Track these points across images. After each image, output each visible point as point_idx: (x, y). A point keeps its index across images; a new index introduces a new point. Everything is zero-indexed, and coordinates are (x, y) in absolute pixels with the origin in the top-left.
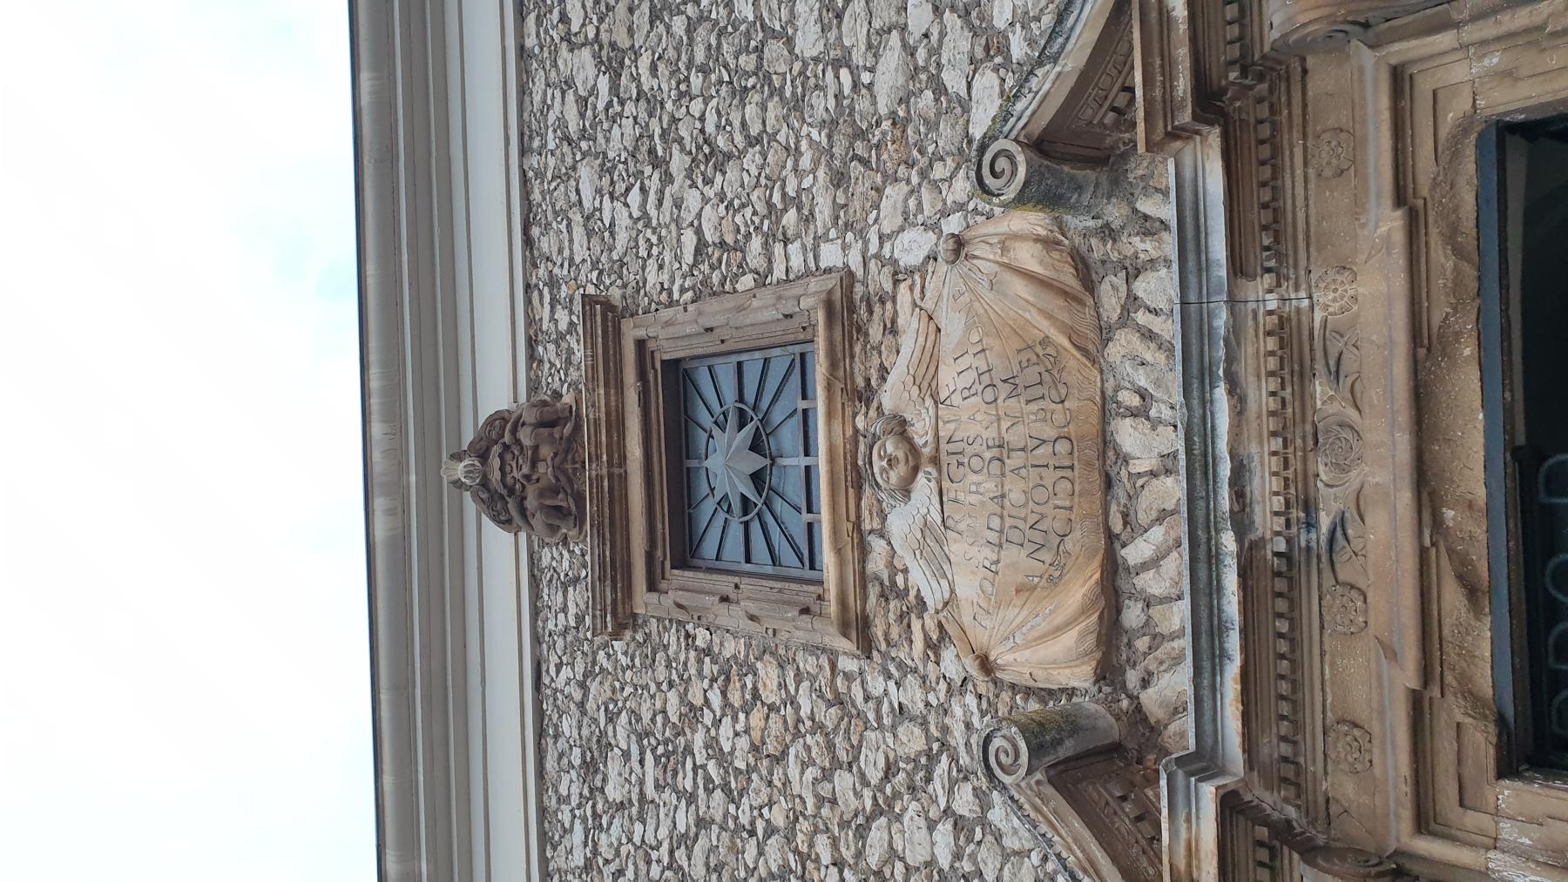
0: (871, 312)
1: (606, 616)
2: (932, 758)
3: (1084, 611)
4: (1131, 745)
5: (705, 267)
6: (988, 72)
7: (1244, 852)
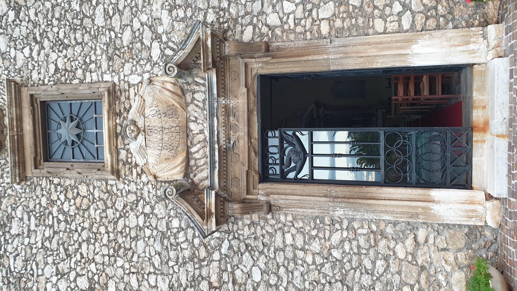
0: (121, 94)
1: (16, 178)
2: (138, 201)
3: (182, 162)
4: (192, 189)
5: (59, 76)
6: (156, 42)
7: (219, 203)
